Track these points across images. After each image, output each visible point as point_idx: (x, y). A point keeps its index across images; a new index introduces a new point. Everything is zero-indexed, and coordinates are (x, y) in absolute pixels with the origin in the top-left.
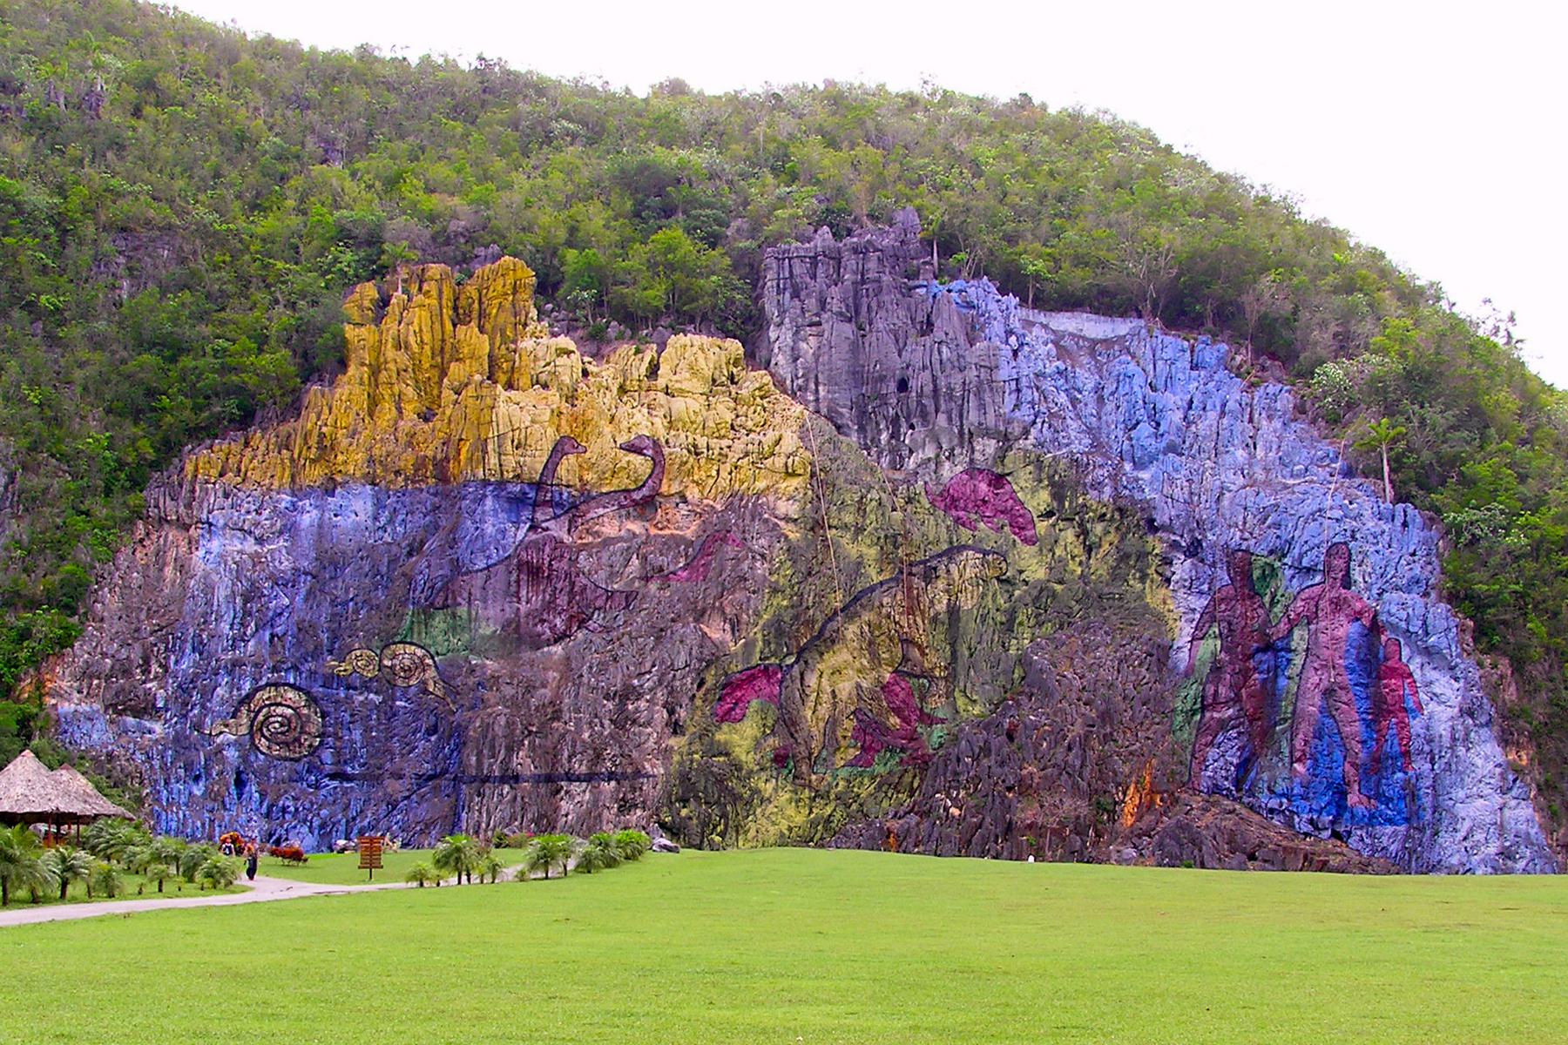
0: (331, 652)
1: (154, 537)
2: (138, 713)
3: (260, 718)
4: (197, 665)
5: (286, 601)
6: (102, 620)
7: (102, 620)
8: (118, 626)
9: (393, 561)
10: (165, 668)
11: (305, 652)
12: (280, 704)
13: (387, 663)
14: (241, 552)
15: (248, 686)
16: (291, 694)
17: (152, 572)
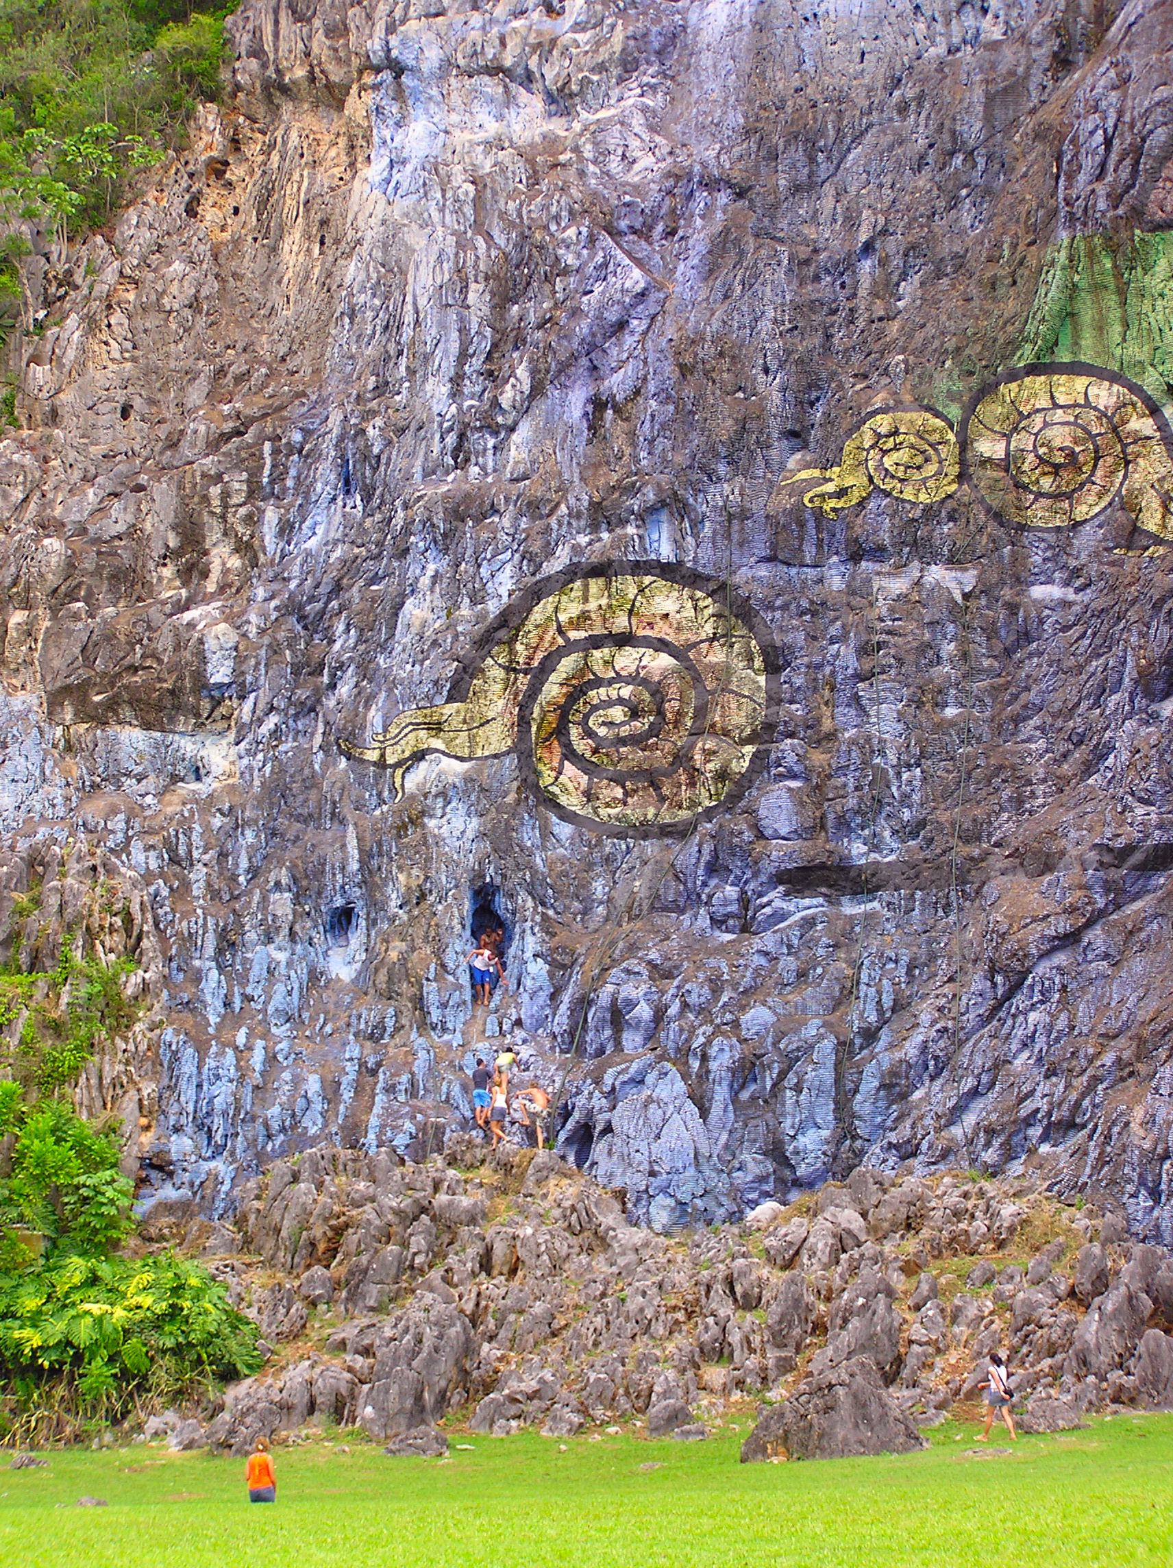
0: (796, 436)
1: (253, 150)
2: (158, 711)
3: (552, 690)
4: (353, 532)
5: (636, 278)
6: (54, 416)
7: (54, 416)
8: (113, 434)
9: (1005, 94)
10: (246, 548)
11: (717, 444)
12: (625, 640)
13: (989, 447)
14: (495, 144)
15: (504, 584)
16: (666, 600)
17: (249, 263)
